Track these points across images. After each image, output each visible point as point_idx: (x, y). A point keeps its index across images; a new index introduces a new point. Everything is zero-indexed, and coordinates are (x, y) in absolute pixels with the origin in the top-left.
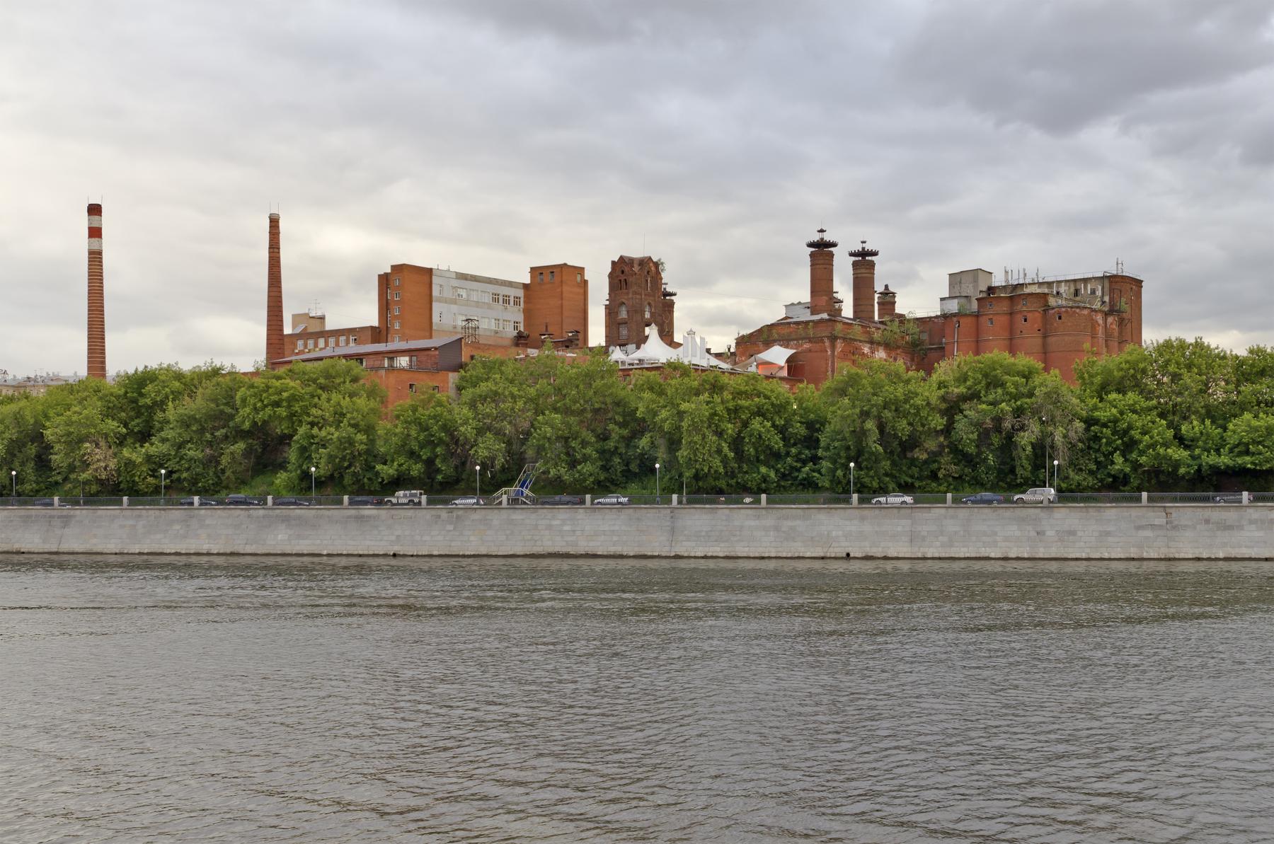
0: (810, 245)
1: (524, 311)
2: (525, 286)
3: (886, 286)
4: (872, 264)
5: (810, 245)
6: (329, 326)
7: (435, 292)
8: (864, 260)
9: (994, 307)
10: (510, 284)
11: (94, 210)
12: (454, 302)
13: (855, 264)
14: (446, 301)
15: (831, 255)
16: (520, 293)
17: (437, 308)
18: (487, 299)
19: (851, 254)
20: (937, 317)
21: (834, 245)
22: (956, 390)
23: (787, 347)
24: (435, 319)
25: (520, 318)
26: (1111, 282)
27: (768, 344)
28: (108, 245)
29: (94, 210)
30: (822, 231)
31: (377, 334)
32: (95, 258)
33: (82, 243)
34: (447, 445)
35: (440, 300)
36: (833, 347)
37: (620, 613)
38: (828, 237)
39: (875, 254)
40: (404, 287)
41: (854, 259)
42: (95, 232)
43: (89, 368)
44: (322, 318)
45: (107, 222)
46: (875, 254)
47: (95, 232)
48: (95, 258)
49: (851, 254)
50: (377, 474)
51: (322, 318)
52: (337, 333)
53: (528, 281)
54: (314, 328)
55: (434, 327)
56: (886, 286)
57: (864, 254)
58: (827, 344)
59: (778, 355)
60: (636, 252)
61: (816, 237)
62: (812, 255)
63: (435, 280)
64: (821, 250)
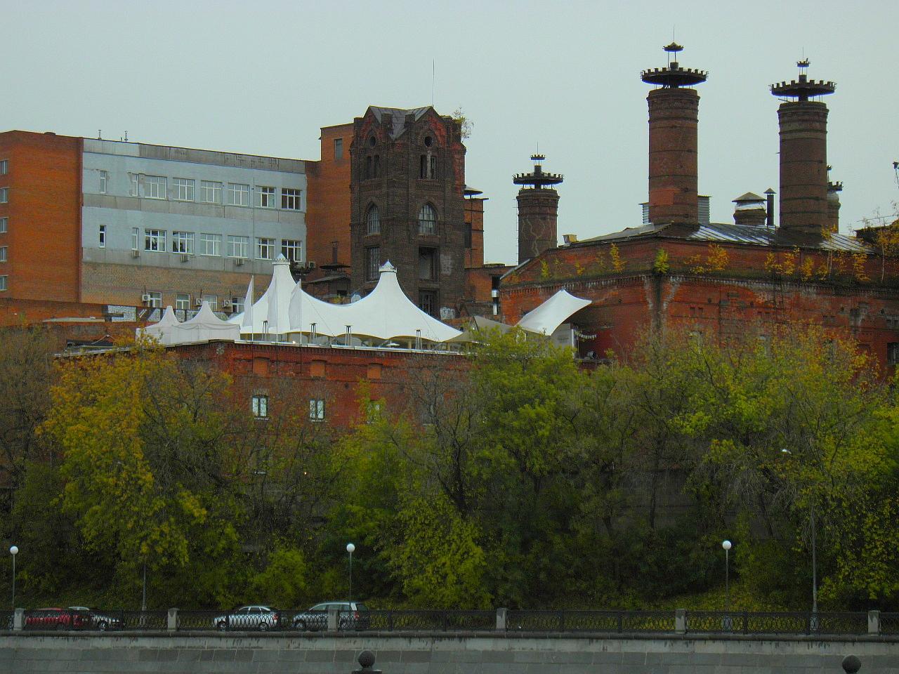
0: (648, 77)
2: (310, 167)
4: (822, 111)
5: (648, 77)
7: (90, 185)
10: (274, 164)
12: (137, 204)
13: (784, 112)
14: (115, 203)
15: (693, 99)
16: (299, 182)
17: (91, 219)
19: (777, 91)
21: (698, 78)
22: (651, 306)
23: (866, 235)
24: (89, 238)
30: (673, 48)
35: (100, 202)
36: (658, 295)
38: (686, 62)
39: (827, 89)
46: (827, 89)
49: (777, 91)
50: (108, 435)
53: (316, 156)
55: (86, 257)
57: (803, 88)
58: (647, 287)
60: (405, 97)
61: (662, 62)
62: (652, 98)
63: (88, 161)
64: (673, 95)
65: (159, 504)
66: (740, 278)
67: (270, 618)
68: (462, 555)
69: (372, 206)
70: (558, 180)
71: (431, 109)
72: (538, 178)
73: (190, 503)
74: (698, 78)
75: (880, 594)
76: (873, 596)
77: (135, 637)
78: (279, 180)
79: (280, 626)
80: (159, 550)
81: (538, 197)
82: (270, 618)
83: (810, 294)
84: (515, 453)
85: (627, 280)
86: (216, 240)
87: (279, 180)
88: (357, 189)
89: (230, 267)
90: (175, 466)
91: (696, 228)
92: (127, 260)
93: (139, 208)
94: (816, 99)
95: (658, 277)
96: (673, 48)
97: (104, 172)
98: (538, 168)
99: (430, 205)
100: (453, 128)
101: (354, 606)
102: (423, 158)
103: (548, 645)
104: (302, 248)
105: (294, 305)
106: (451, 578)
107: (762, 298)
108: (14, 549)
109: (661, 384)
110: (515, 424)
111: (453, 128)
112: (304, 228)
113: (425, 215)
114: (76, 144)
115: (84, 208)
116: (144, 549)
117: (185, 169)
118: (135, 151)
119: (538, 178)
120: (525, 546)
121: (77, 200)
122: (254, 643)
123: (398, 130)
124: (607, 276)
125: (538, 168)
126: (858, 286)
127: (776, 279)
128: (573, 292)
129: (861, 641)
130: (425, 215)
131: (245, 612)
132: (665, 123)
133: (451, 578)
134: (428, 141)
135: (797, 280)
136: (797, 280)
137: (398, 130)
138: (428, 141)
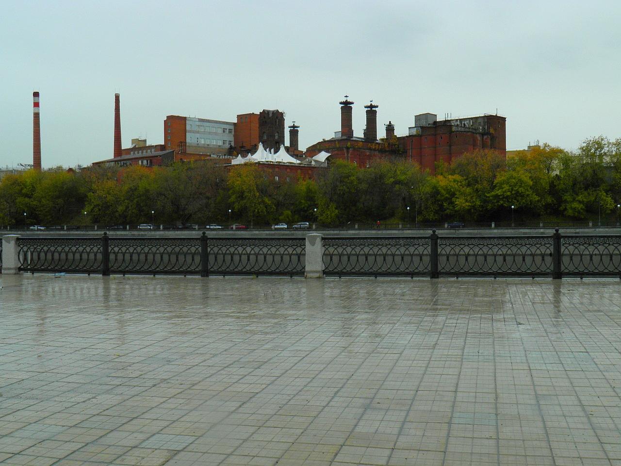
0: (341, 103)
1: (234, 136)
2: (234, 124)
3: (390, 122)
4: (375, 112)
5: (341, 103)
6: (148, 144)
7: (188, 128)
8: (371, 113)
9: (434, 134)
11: (36, 95)
12: (198, 132)
13: (367, 112)
14: (194, 132)
15: (351, 108)
16: (232, 127)
18: (220, 131)
19: (365, 107)
20: (407, 136)
21: (352, 103)
25: (232, 139)
26: (487, 119)
27: (320, 151)
28: (42, 110)
29: (36, 95)
30: (346, 96)
31: (162, 148)
32: (37, 116)
33: (31, 110)
34: (306, 211)
35: (190, 132)
36: (348, 152)
37: (426, 309)
38: (349, 100)
39: (377, 107)
40: (175, 125)
41: (367, 109)
42: (36, 105)
43: (34, 161)
44: (145, 141)
45: (41, 100)
46: (377, 107)
47: (36, 105)
48: (37, 116)
49: (365, 107)
51: (145, 141)
52: (151, 147)
54: (141, 145)
55: (187, 145)
56: (390, 122)
57: (371, 106)
58: (345, 151)
59: (322, 156)
60: (271, 108)
61: (344, 100)
63: (187, 122)
64: (347, 107)
65: (260, 200)
66: (364, 149)
67: (286, 226)
68: (333, 212)
69: (264, 132)
70: (299, 127)
71: (278, 110)
72: (294, 127)
73: (266, 200)
74: (352, 103)
75: (432, 219)
76: (431, 220)
77: (264, 231)
78: (228, 127)
79: (288, 228)
80: (260, 211)
81: (390, 129)
82: (286, 226)
83: (377, 153)
84: (348, 188)
85: (340, 149)
86: (214, 141)
87: (228, 127)
88: (260, 128)
89: (218, 147)
90: (263, 191)
91: (352, 137)
92: (196, 145)
93: (198, 133)
94: (374, 109)
95: (348, 148)
96: (346, 96)
97: (191, 125)
98: (294, 124)
99: (278, 132)
100: (503, 120)
101: (308, 224)
102: (276, 121)
103: (368, 231)
104: (233, 142)
105: (263, 154)
106: (329, 217)
107: (368, 154)
108: (153, 212)
109: (247, 171)
110: (348, 181)
111: (503, 120)
112: (233, 138)
113: (276, 134)
114: (185, 118)
115: (187, 134)
116: (256, 211)
117: (208, 124)
118: (197, 120)
119: (294, 127)
120: (345, 210)
121: (185, 131)
122: (294, 232)
123: (271, 115)
124: (334, 148)
125: (294, 124)
126: (386, 151)
127: (370, 149)
128: (326, 152)
129: (587, 228)
130: (276, 134)
131: (280, 225)
132: (345, 114)
133: (329, 217)
134: (277, 118)
135: (375, 150)
136: (375, 150)
137: (271, 115)
138: (277, 118)
